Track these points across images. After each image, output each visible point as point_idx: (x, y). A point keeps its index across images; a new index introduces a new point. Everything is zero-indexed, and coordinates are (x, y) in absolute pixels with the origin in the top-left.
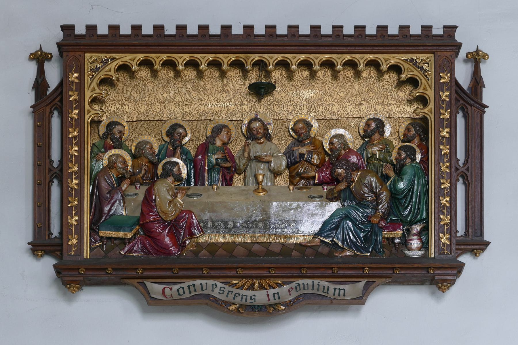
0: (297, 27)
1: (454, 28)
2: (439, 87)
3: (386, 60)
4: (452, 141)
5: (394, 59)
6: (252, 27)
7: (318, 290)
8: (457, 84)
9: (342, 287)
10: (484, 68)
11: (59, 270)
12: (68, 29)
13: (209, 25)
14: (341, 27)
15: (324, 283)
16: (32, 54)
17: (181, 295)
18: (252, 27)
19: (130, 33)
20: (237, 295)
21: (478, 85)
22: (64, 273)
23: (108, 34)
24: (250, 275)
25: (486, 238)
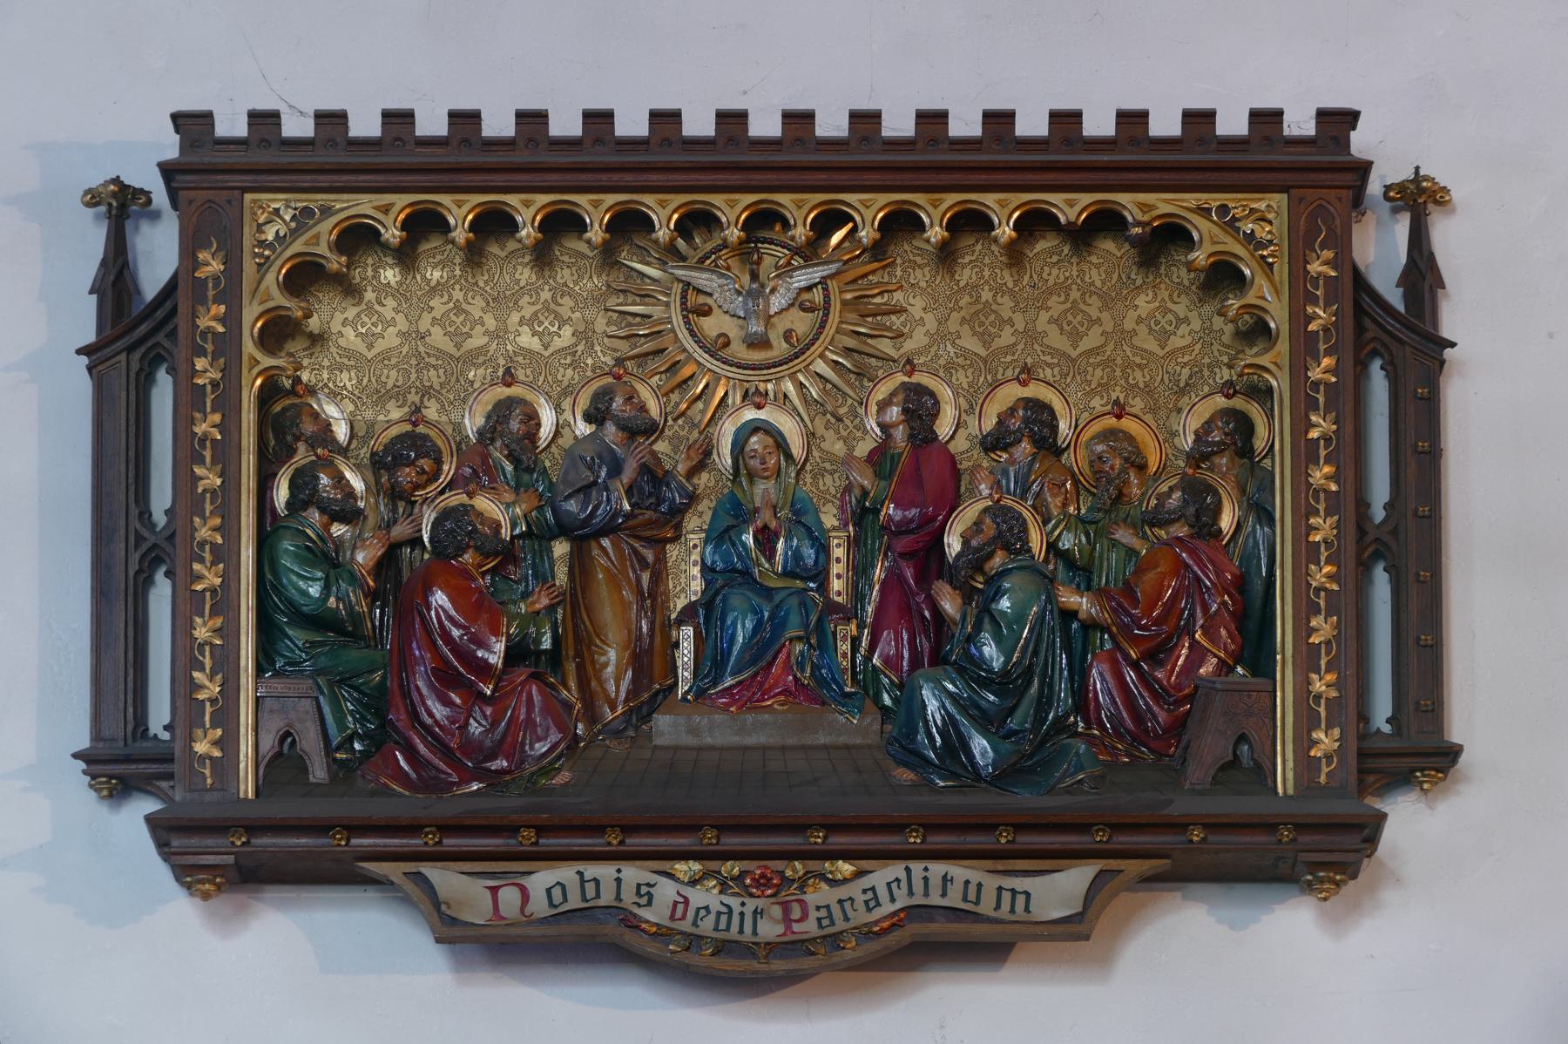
0: (1209, 116)
1: (1349, 118)
2: (1301, 291)
3: (1144, 207)
4: (188, 451)
5: (1164, 204)
6: (874, 117)
7: (926, 894)
8: (1359, 282)
9: (1020, 883)
10: (1446, 236)
11: (163, 830)
12: (192, 124)
13: (547, 110)
14: (1276, 116)
15: (959, 872)
16: (87, 192)
17: (556, 907)
18: (874, 117)
19: (780, 135)
20: (703, 912)
21: (1424, 279)
22: (177, 842)
23: (514, 138)
24: (870, 847)
25: (1457, 732)
